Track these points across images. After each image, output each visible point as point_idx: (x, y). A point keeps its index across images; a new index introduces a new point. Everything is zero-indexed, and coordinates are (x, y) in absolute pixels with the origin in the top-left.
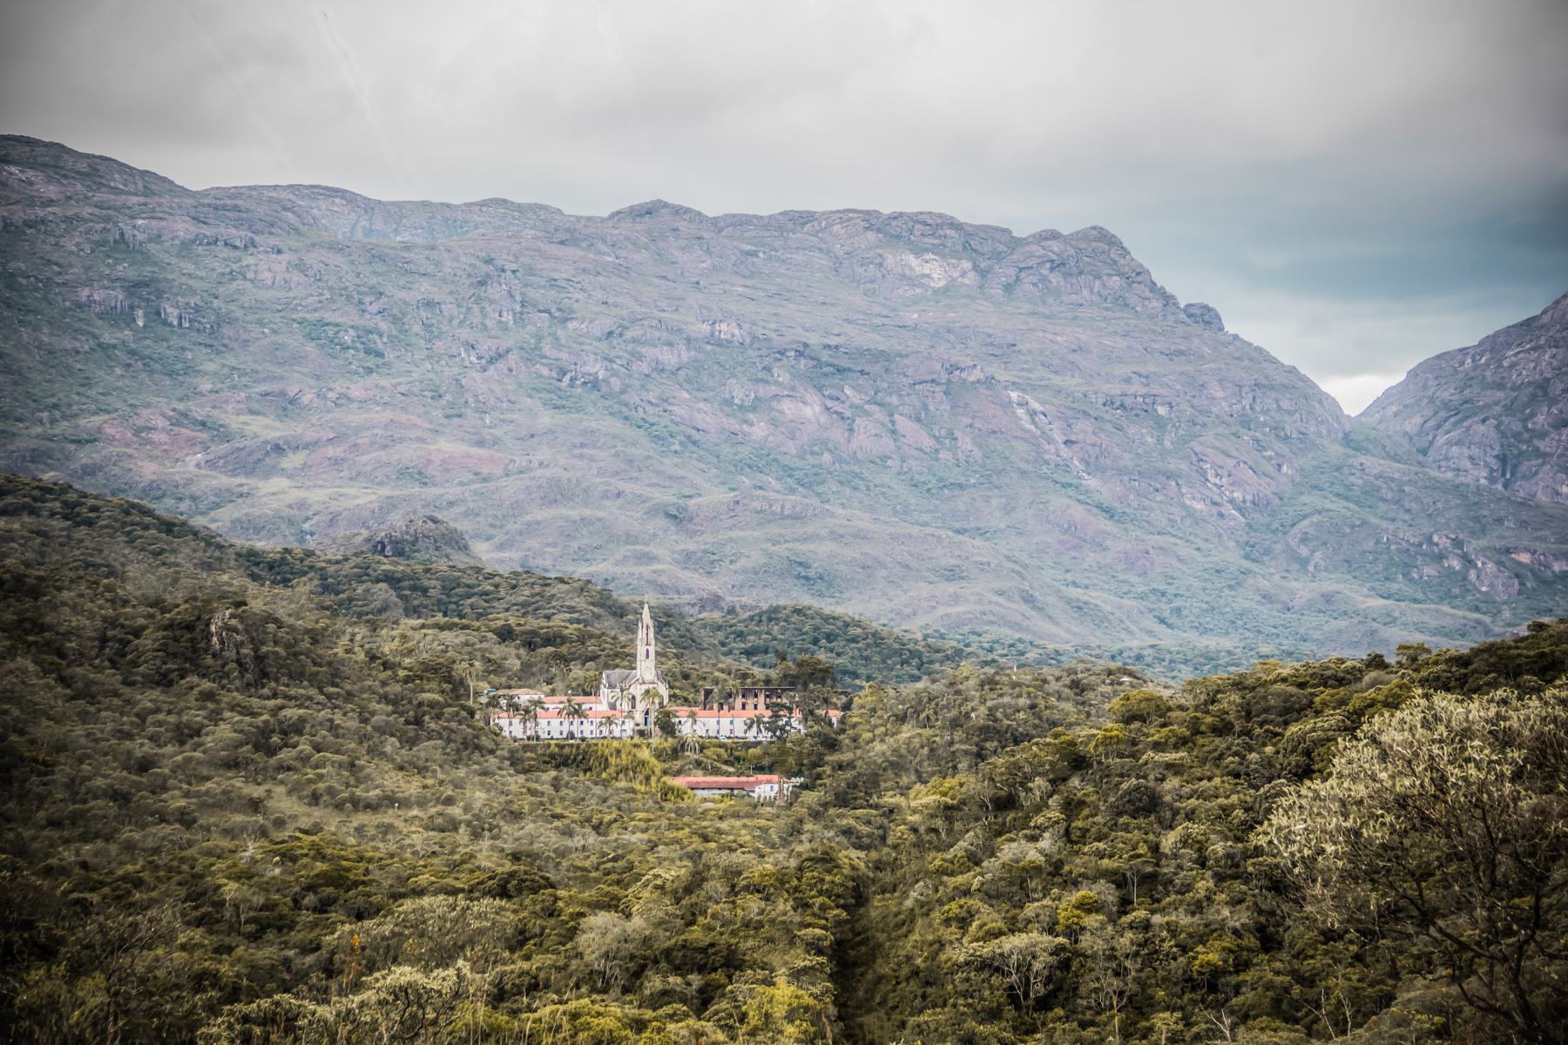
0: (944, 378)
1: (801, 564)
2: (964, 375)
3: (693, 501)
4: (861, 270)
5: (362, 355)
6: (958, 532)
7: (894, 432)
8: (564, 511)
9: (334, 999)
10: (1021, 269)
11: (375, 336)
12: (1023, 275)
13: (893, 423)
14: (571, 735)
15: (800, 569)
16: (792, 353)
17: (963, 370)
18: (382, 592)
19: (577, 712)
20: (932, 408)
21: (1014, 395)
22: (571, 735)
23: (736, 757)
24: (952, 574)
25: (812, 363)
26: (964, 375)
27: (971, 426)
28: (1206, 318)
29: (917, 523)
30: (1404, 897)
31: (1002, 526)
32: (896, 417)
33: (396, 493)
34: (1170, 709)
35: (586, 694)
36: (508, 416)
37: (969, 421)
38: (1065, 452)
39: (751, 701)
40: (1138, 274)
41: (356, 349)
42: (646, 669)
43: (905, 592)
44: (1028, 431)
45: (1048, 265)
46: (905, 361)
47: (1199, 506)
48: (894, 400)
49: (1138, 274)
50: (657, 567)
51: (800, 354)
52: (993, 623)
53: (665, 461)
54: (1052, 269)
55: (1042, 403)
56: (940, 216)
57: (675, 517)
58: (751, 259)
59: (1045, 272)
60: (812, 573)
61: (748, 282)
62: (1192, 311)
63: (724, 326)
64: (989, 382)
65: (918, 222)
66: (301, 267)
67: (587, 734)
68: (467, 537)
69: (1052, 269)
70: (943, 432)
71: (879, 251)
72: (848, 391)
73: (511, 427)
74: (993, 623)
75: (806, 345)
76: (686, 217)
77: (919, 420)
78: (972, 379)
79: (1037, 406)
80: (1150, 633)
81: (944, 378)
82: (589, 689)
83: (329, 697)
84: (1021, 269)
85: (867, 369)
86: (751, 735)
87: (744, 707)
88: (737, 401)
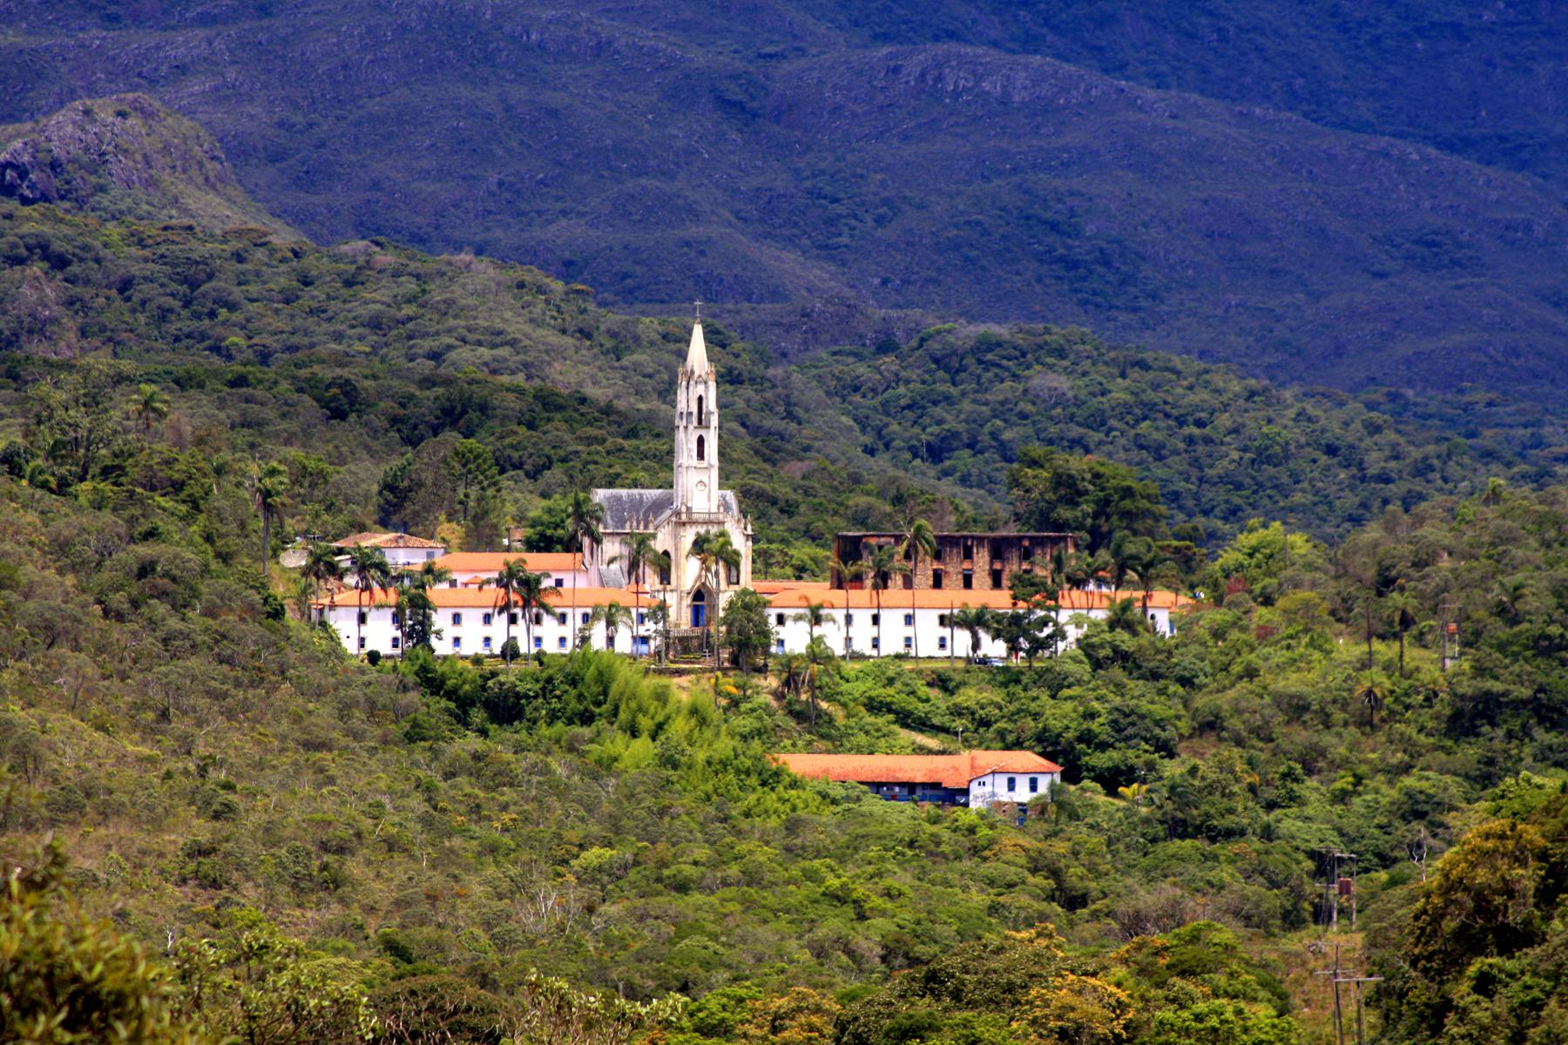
1: (1054, 227)
3: (785, 67)
6: (1448, 145)
8: (465, 92)
14: (510, 652)
15: (1052, 239)
22: (510, 652)
23: (908, 702)
24: (1431, 251)
29: (1344, 124)
30: (267, 531)
33: (33, 42)
39: (954, 568)
42: (700, 486)
43: (1315, 296)
50: (693, 231)
52: (1535, 375)
57: (740, 106)
60: (1079, 249)
66: (1218, 391)
67: (550, 647)
74: (1535, 375)
87: (937, 583)
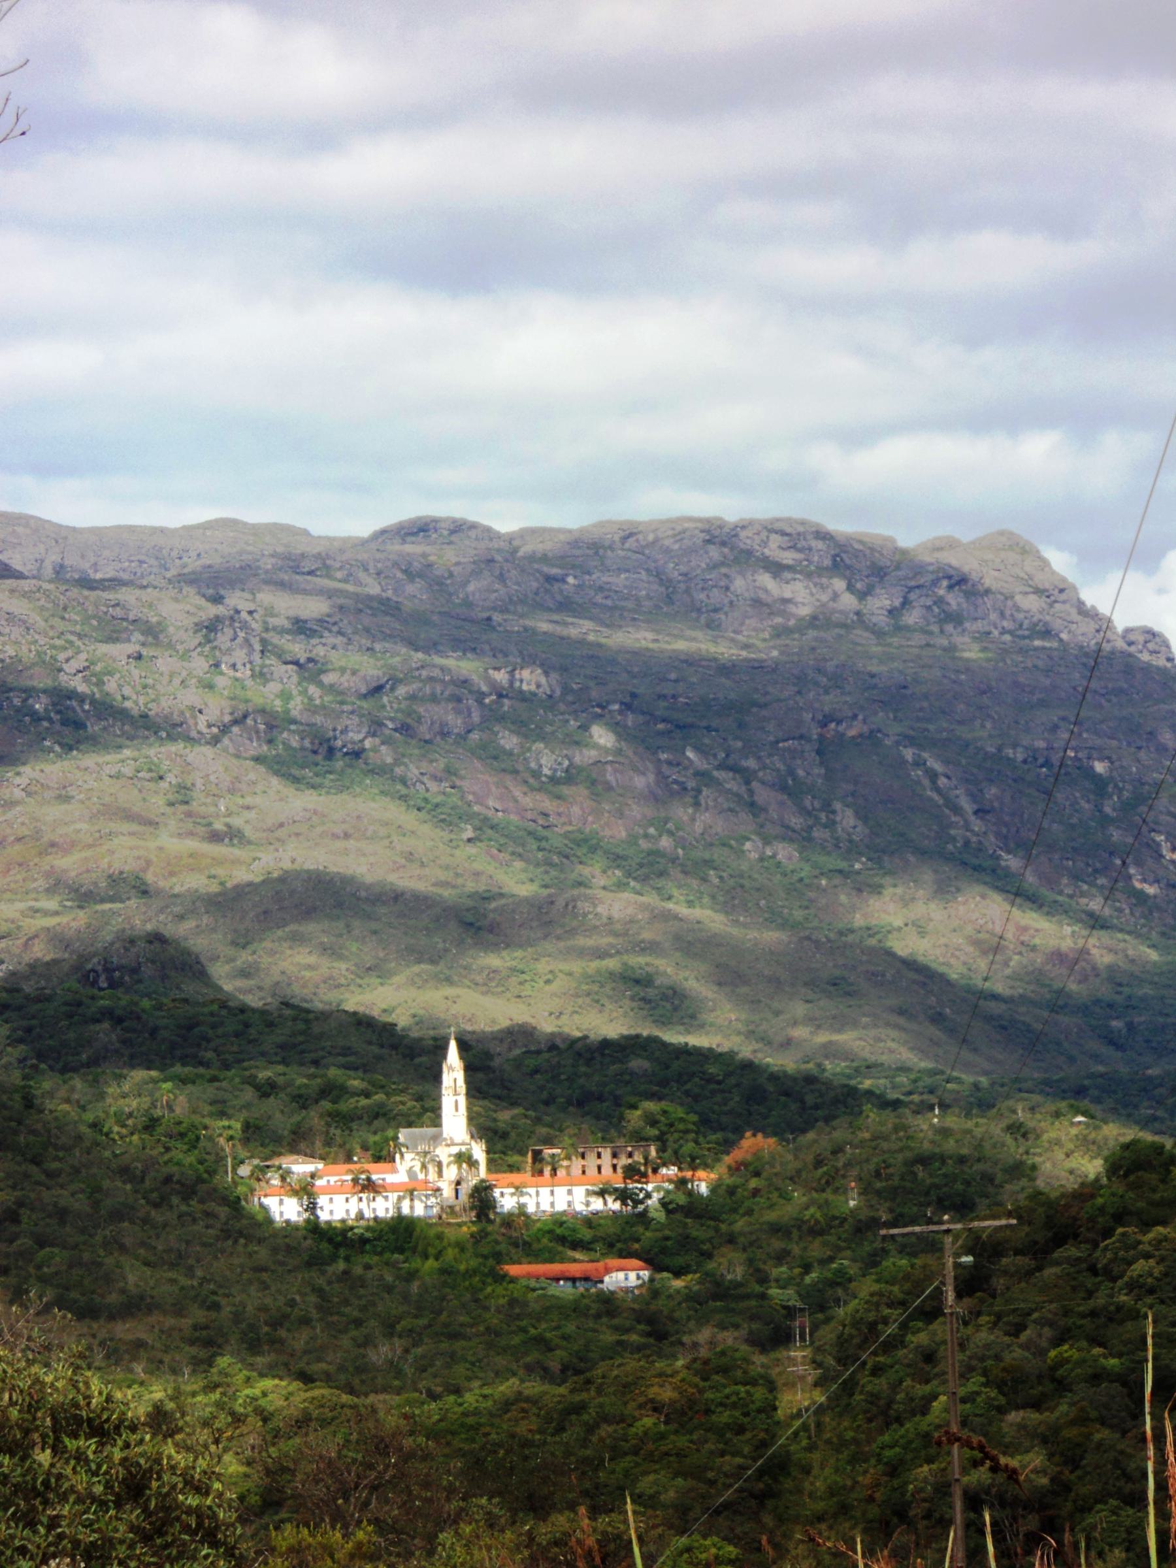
0: (815, 732)
2: (841, 728)
4: (702, 596)
5: (58, 727)
7: (752, 804)
9: (1041, 1210)
10: (911, 589)
11: (74, 703)
12: (912, 596)
13: (751, 792)
14: (360, 1216)
16: (616, 707)
17: (839, 722)
18: (104, 1032)
19: (370, 1187)
20: (801, 773)
21: (909, 754)
22: (360, 1216)
25: (641, 719)
26: (841, 728)
27: (853, 794)
28: (1151, 646)
31: (898, 923)
32: (754, 784)
34: (11, 690)
35: (378, 1159)
36: (249, 800)
37: (851, 787)
38: (977, 825)
40: (1061, 591)
41: (50, 720)
44: (930, 799)
45: (945, 583)
46: (764, 713)
47: (1151, 890)
48: (751, 763)
49: (1061, 591)
51: (627, 707)
53: (457, 852)
54: (950, 587)
55: (946, 762)
56: (803, 523)
57: (471, 924)
58: (556, 586)
59: (941, 592)
61: (556, 617)
62: (1132, 637)
63: (526, 674)
64: (872, 737)
65: (772, 531)
68: (203, 959)
69: (950, 587)
70: (817, 804)
71: (724, 570)
72: (690, 754)
73: (252, 815)
75: (634, 695)
76: (473, 534)
77: (784, 788)
78: (852, 733)
79: (938, 766)
80: (1096, 1057)
81: (815, 732)
82: (384, 1155)
83: (50, 1175)
84: (911, 589)
85: (714, 724)
86: (597, 1204)
88: (546, 771)
